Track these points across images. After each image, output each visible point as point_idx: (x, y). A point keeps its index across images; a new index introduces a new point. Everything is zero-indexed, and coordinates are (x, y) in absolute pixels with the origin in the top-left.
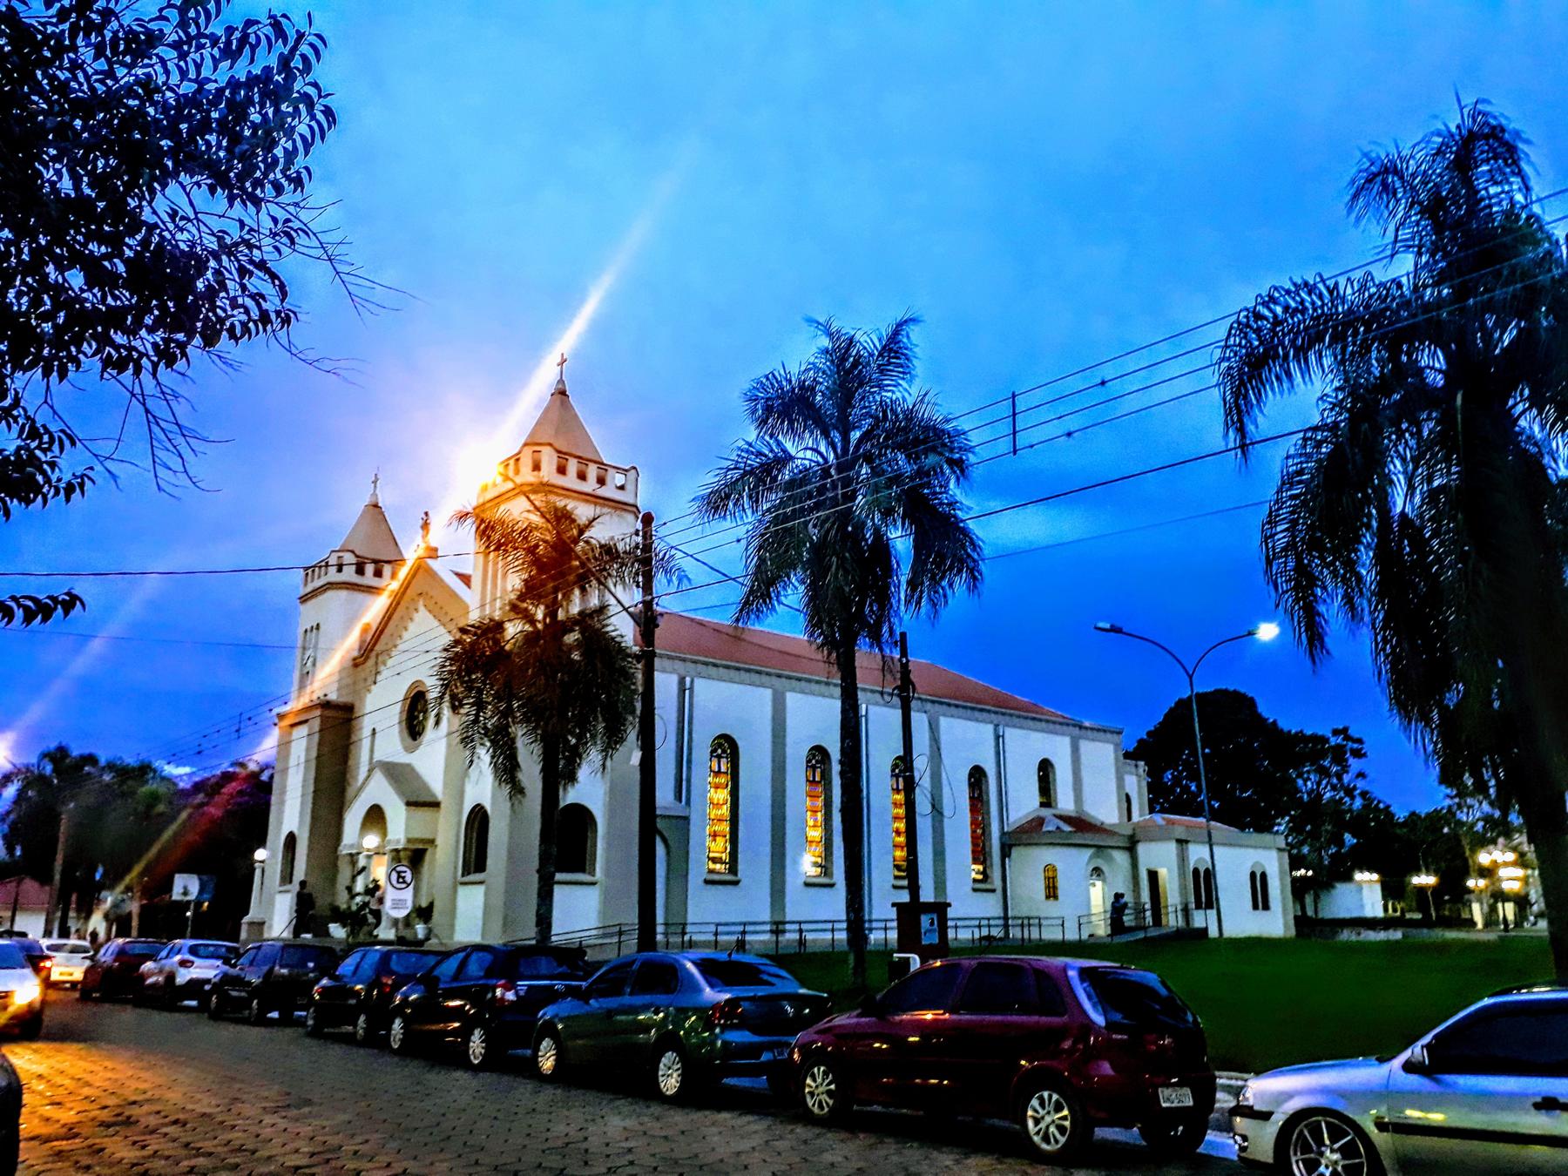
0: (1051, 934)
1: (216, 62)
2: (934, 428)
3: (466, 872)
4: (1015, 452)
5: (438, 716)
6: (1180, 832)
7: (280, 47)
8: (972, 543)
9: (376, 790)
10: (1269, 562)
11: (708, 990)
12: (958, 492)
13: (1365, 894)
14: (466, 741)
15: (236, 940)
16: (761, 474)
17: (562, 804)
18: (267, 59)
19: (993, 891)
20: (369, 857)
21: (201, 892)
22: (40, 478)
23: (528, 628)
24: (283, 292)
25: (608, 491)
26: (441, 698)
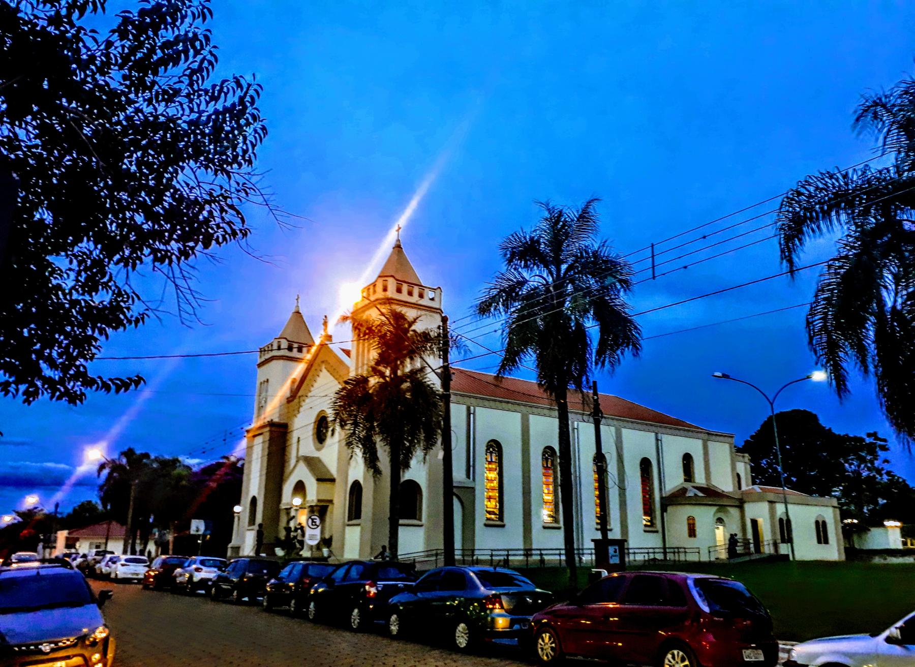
0: (692, 558)
1: (207, 103)
2: (612, 262)
3: (350, 519)
4: (654, 277)
5: (333, 431)
6: (771, 496)
7: (239, 93)
8: (636, 328)
9: (299, 473)
10: (811, 338)
11: (482, 588)
12: (625, 297)
13: (890, 535)
14: (349, 444)
15: (225, 557)
16: (510, 293)
17: (402, 480)
18: (232, 99)
19: (657, 532)
20: (297, 510)
21: (206, 530)
22: (122, 317)
23: (381, 380)
24: (243, 221)
25: (425, 302)
26: (335, 420)
